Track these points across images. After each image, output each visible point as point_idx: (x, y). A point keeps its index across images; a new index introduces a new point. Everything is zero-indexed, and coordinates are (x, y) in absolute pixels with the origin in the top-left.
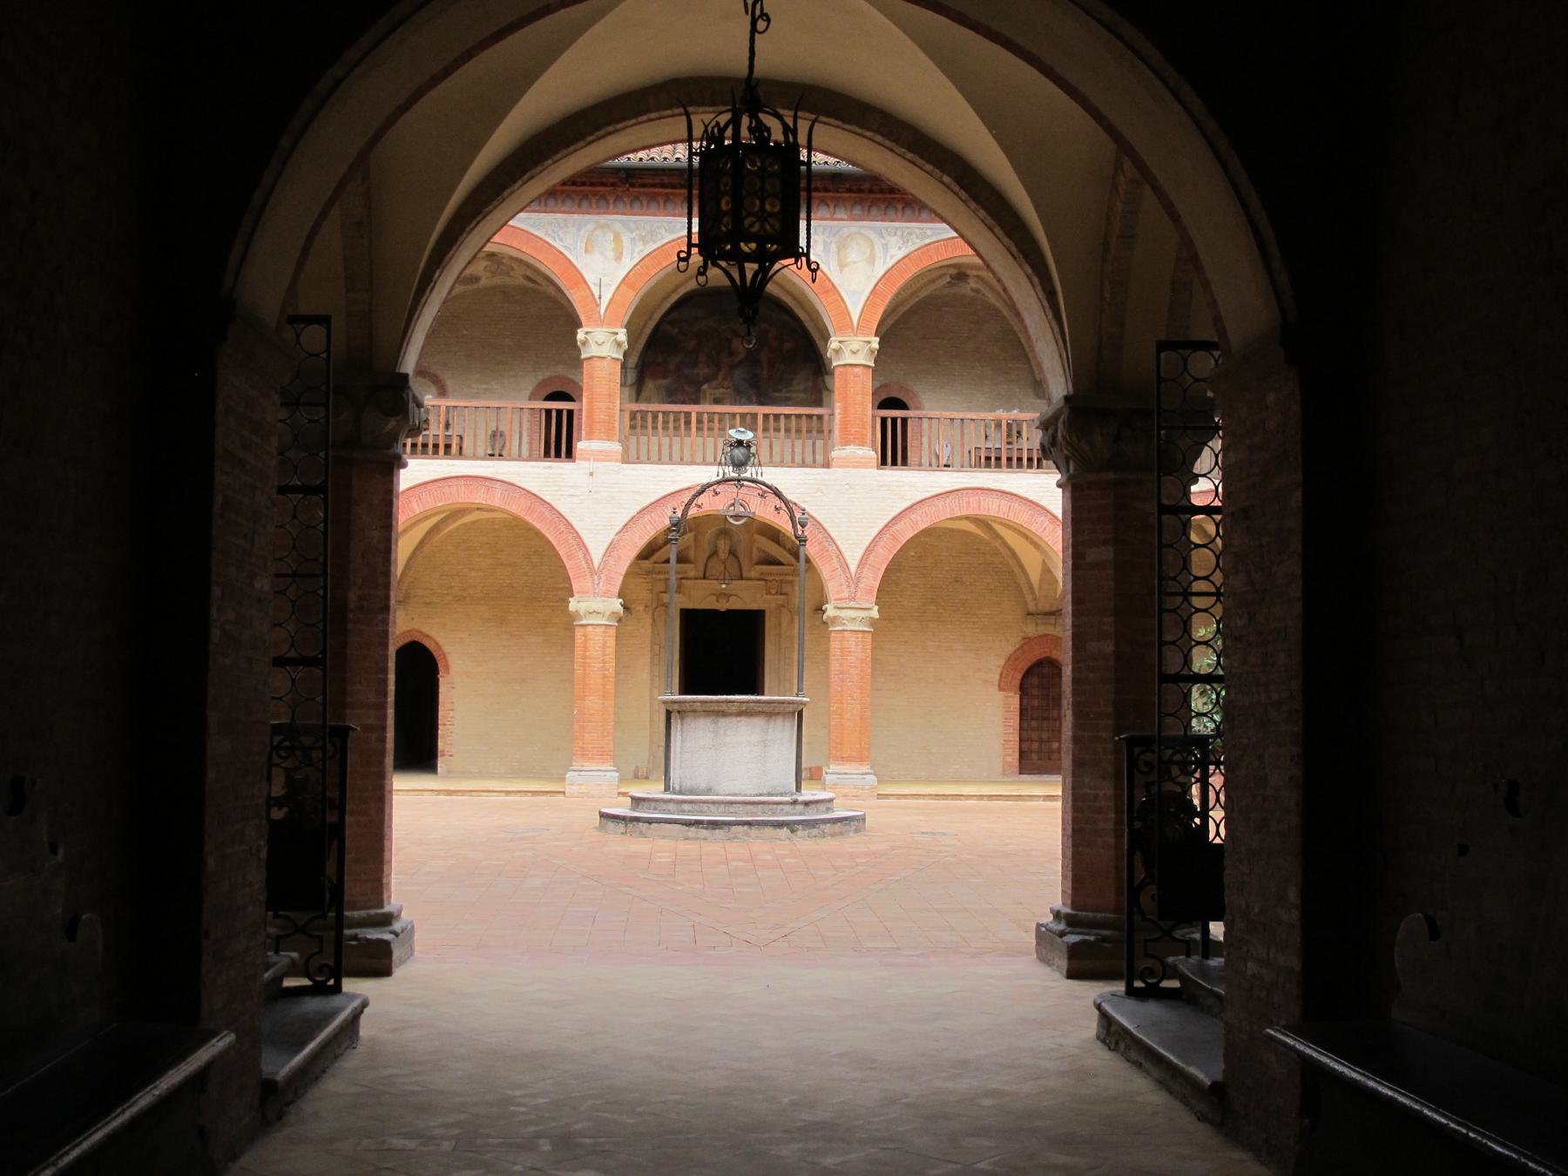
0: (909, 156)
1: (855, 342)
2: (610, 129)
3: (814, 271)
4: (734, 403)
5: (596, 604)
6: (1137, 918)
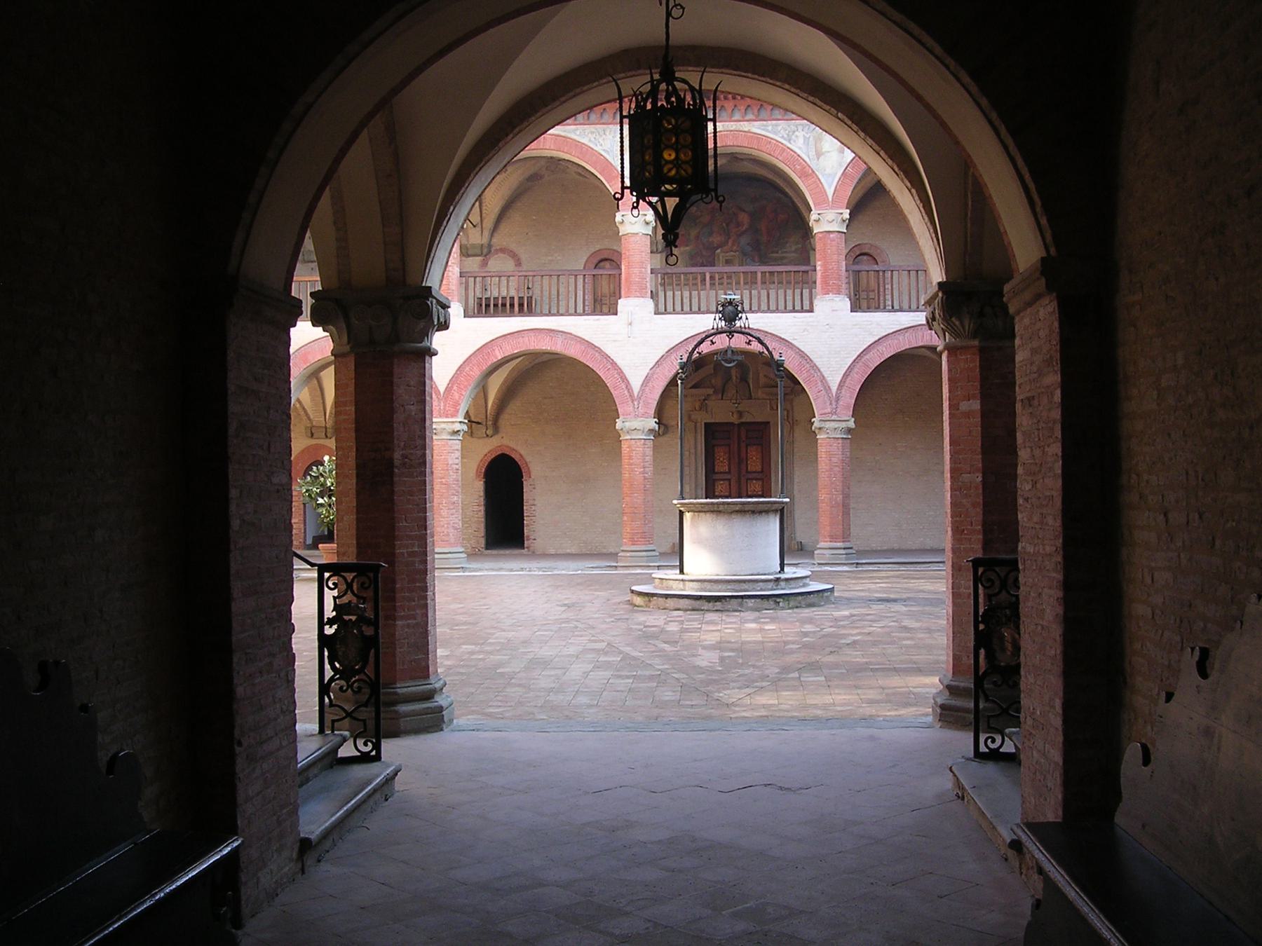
0: (811, 98)
1: (830, 215)
2: (578, 90)
3: (721, 203)
4: (741, 265)
5: (636, 424)
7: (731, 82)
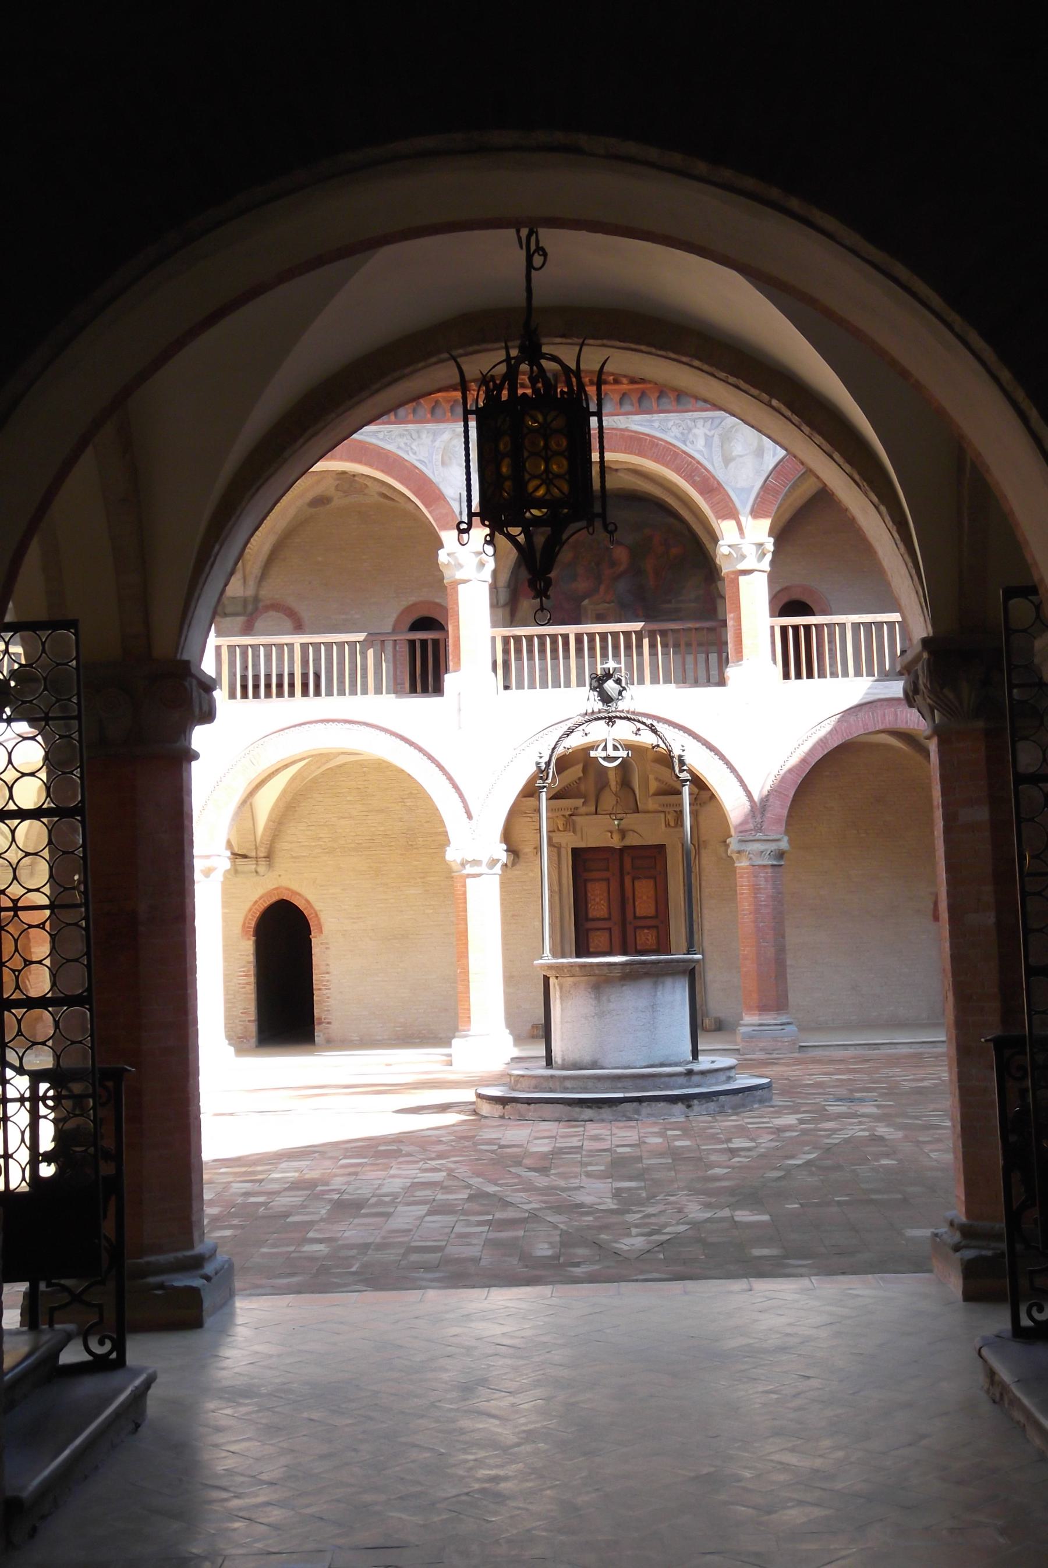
0: (732, 379)
3: (611, 533)
6: (1019, 1247)
7: (623, 361)
